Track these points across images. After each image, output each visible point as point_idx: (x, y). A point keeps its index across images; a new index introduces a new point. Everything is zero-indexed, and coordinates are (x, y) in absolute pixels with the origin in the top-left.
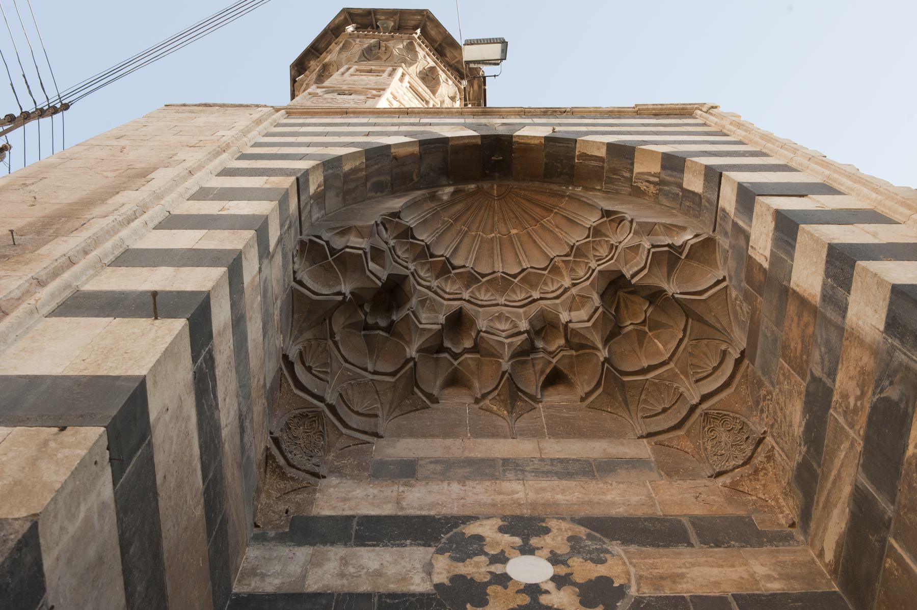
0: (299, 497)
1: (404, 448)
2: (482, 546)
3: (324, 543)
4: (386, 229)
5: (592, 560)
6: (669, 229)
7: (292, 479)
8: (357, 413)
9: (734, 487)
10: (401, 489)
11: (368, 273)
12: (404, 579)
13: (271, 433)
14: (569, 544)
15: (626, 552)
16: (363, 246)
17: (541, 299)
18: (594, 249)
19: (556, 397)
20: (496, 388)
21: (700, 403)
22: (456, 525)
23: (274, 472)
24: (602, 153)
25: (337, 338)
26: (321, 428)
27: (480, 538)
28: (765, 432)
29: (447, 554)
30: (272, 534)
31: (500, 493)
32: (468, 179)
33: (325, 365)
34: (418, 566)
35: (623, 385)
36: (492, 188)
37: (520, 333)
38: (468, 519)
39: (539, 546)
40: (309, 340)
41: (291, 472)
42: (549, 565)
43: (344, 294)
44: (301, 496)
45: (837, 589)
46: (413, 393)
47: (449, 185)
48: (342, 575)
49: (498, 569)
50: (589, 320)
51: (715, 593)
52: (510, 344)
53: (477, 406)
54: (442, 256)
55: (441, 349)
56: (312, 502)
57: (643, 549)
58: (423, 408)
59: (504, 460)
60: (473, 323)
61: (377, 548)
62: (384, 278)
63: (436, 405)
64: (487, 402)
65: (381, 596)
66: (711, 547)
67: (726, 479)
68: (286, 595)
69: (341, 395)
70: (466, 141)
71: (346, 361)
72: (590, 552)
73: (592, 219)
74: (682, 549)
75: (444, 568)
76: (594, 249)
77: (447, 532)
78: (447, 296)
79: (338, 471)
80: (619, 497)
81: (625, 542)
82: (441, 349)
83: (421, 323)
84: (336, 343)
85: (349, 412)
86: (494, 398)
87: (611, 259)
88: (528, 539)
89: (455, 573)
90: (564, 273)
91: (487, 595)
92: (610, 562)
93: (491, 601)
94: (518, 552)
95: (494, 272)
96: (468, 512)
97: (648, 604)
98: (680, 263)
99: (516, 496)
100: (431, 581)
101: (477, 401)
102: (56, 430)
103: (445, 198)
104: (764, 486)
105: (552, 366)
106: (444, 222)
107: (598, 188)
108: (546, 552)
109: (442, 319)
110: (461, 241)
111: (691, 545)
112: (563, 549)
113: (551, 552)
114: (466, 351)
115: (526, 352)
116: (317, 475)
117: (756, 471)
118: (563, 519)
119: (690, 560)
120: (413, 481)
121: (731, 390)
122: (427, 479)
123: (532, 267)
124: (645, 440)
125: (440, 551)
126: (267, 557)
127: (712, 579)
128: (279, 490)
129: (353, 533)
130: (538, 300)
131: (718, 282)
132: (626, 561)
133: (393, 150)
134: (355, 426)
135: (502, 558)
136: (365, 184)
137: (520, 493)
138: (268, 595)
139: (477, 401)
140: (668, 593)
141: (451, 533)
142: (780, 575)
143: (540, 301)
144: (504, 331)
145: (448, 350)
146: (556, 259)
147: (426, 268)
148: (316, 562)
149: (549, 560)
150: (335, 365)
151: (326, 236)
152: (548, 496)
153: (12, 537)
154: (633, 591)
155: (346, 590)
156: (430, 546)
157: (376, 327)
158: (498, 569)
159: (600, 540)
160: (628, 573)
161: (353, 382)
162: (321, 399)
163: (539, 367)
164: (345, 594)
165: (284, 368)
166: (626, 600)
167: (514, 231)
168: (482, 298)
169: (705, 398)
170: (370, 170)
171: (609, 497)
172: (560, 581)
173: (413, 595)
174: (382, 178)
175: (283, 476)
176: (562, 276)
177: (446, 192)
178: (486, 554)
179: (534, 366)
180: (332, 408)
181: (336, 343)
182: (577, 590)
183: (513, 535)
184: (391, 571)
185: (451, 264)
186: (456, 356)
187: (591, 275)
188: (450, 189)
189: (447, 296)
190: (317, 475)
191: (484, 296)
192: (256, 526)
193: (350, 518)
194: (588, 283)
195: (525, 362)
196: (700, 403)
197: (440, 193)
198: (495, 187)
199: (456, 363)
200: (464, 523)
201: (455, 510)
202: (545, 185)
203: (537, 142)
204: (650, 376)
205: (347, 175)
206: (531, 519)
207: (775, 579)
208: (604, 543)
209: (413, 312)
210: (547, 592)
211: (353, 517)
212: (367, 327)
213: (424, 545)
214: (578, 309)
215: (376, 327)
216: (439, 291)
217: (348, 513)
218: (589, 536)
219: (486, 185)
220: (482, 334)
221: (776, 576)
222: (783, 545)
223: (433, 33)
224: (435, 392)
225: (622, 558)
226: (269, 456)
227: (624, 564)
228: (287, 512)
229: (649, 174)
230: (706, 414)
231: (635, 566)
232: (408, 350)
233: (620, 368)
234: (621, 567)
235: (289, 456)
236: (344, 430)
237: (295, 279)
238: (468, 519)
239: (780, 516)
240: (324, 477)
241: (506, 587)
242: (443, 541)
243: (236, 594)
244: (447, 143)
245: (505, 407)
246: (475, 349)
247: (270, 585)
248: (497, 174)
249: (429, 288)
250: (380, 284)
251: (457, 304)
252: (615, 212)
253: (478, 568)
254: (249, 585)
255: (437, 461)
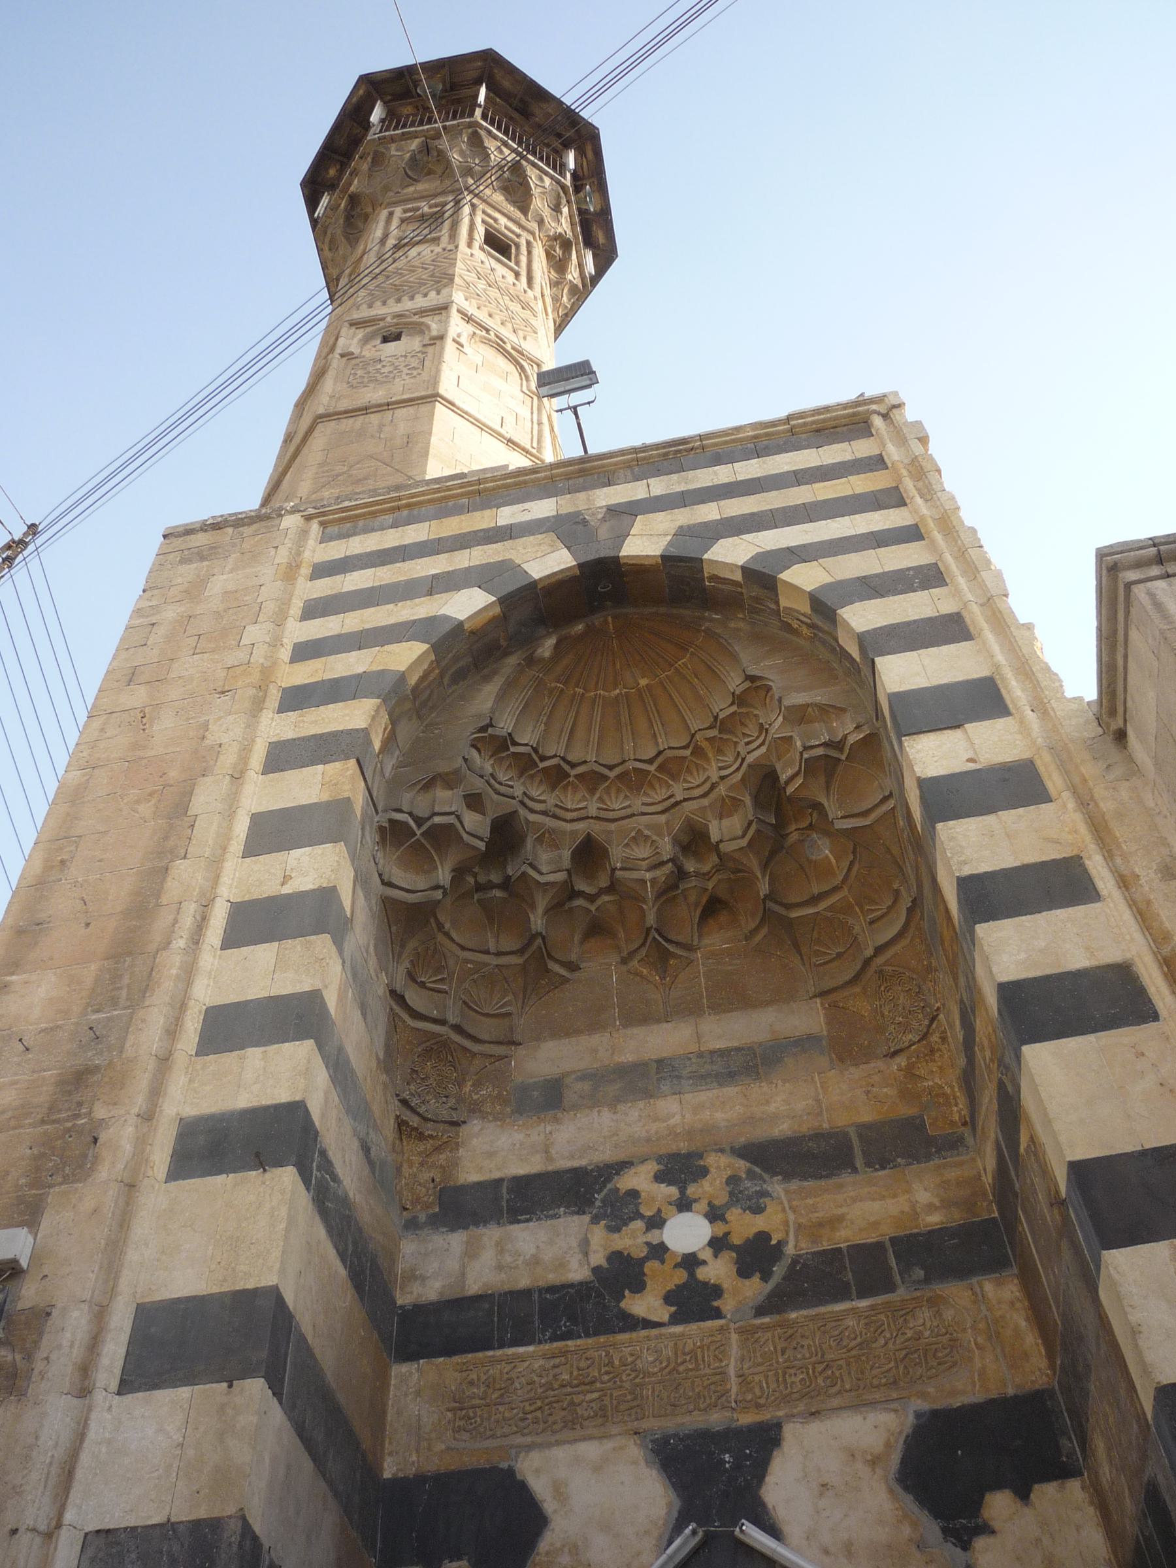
0: (442, 1158)
1: (547, 1058)
2: (637, 1205)
3: (476, 1224)
4: (479, 750)
5: (750, 1208)
6: (825, 711)
7: (431, 1137)
8: (487, 1015)
9: (910, 1072)
10: (549, 1128)
11: (465, 836)
12: (562, 1265)
13: (397, 1095)
14: (728, 1189)
15: (787, 1191)
16: (453, 809)
17: (685, 800)
18: (742, 724)
19: (717, 940)
20: (643, 944)
21: (875, 956)
22: (609, 1179)
23: (410, 1136)
24: (738, 577)
25: (447, 926)
26: (450, 1058)
27: (634, 1194)
28: (938, 1009)
29: (603, 1223)
30: (422, 1217)
31: (656, 1119)
32: (572, 618)
33: (439, 970)
34: (574, 1244)
35: (789, 924)
36: (606, 622)
37: (663, 863)
38: (622, 1166)
39: (697, 1196)
40: (415, 949)
41: (429, 1129)
42: (706, 1223)
43: (443, 887)
44: (443, 1157)
45: (996, 1215)
46: (547, 970)
47: (549, 635)
48: (500, 1268)
49: (654, 1237)
50: (743, 836)
51: (872, 1239)
52: (653, 881)
53: (624, 968)
54: (555, 756)
55: (574, 894)
56: (455, 1163)
57: (806, 1183)
58: (562, 984)
59: (659, 1062)
60: (605, 853)
61: (531, 1224)
62: (486, 832)
63: (577, 974)
64: (634, 963)
65: (540, 1290)
66: (876, 1170)
67: (901, 1061)
68: (449, 1301)
69: (464, 1002)
70: (560, 577)
71: (463, 948)
72: (749, 1198)
73: (735, 683)
74: (846, 1178)
75: (602, 1243)
76: (742, 724)
77: (601, 1190)
78: (569, 816)
79: (475, 1109)
80: (785, 1105)
81: (787, 1176)
82: (574, 894)
83: (542, 874)
84: (447, 935)
85: (478, 1017)
86: (642, 960)
87: (763, 744)
88: (685, 1188)
89: (611, 1249)
90: (710, 755)
91: (645, 1275)
92: (769, 1210)
93: (649, 1283)
94: (674, 1208)
95: (624, 761)
96: (622, 1156)
97: (804, 1265)
98: (840, 768)
99: (672, 1122)
100: (589, 1264)
101: (624, 961)
102: (225, 1385)
103: (547, 654)
104: (941, 1068)
105: (708, 894)
106: (551, 691)
107: (741, 616)
108: (702, 1206)
109: (567, 854)
110: (577, 712)
111: (855, 1170)
112: (721, 1199)
113: (710, 1204)
114: (602, 892)
115: (669, 890)
116: (456, 1124)
117: (932, 1051)
118: (722, 1151)
119: (852, 1194)
120: (560, 1115)
121: (905, 942)
122: (575, 1107)
123: (670, 748)
124: (818, 1000)
125: (595, 1220)
126: (423, 1251)
127: (872, 1219)
128: (420, 1154)
129: (504, 1204)
130: (681, 802)
131: (885, 799)
132: (786, 1205)
133: (466, 626)
134: (486, 1037)
135: (656, 1222)
136: (441, 683)
137: (676, 1114)
138: (432, 1304)
139: (624, 961)
140: (825, 1245)
141: (605, 1191)
142: (942, 1201)
143: (685, 804)
144: (644, 859)
145: (581, 894)
146: (698, 737)
147: (537, 779)
148: (471, 1252)
149: (706, 1216)
150: (451, 962)
151: (406, 799)
152: (706, 1115)
153: (233, 1539)
154: (790, 1249)
155: (506, 1288)
156: (584, 1213)
157: (491, 886)
158: (654, 1237)
159: (761, 1178)
160: (786, 1223)
161: (476, 976)
162: (442, 1022)
163: (692, 898)
164: (506, 1293)
165: (395, 1007)
166: (783, 1263)
167: (643, 682)
168: (617, 806)
169: (879, 950)
170: (443, 664)
171: (772, 1108)
172: (718, 1244)
173: (571, 1286)
174: (462, 663)
175: (421, 1137)
176: (708, 760)
177: (547, 647)
178: (642, 1217)
179: (686, 898)
180: (458, 1029)
181: (447, 935)
182: (734, 1255)
183: (669, 1184)
184: (548, 1255)
185: (568, 763)
186: (592, 898)
187: (741, 765)
188: (551, 642)
189: (569, 816)
190: (456, 1124)
191: (617, 803)
192: (405, 1209)
193: (499, 1182)
194: (739, 775)
195: (674, 897)
196: (875, 956)
197: (539, 651)
198: (610, 619)
199: (593, 908)
200: (617, 1174)
201: (606, 1155)
202: (675, 611)
203: (653, 562)
204: (823, 905)
205: (415, 689)
206: (690, 1156)
207: (937, 1208)
208: (764, 1181)
209: (531, 865)
210: (704, 1262)
211: (501, 1180)
212: (479, 888)
213: (578, 1213)
214: (730, 815)
215: (491, 886)
216: (558, 812)
217: (496, 1175)
218: (751, 1175)
219: (597, 620)
220: (618, 873)
221: (938, 1204)
222: (951, 1156)
223: (506, 84)
224: (573, 957)
225: (782, 1203)
226: (401, 1124)
227: (784, 1210)
228: (433, 1181)
229: (798, 612)
230: (881, 971)
231: (794, 1212)
232: (532, 916)
233: (785, 901)
234: (780, 1216)
235: (421, 1110)
236: (476, 1048)
237: (382, 881)
238: (622, 1166)
239: (955, 1109)
240: (464, 1122)
241: (663, 1262)
242: (598, 1203)
243: (401, 1307)
244: (536, 587)
245: (657, 970)
246: (611, 889)
247: (431, 1291)
248: (609, 603)
249: (544, 813)
250: (481, 845)
251: (580, 826)
252: (761, 678)
253: (635, 1238)
254: (412, 1293)
255: (584, 1077)
